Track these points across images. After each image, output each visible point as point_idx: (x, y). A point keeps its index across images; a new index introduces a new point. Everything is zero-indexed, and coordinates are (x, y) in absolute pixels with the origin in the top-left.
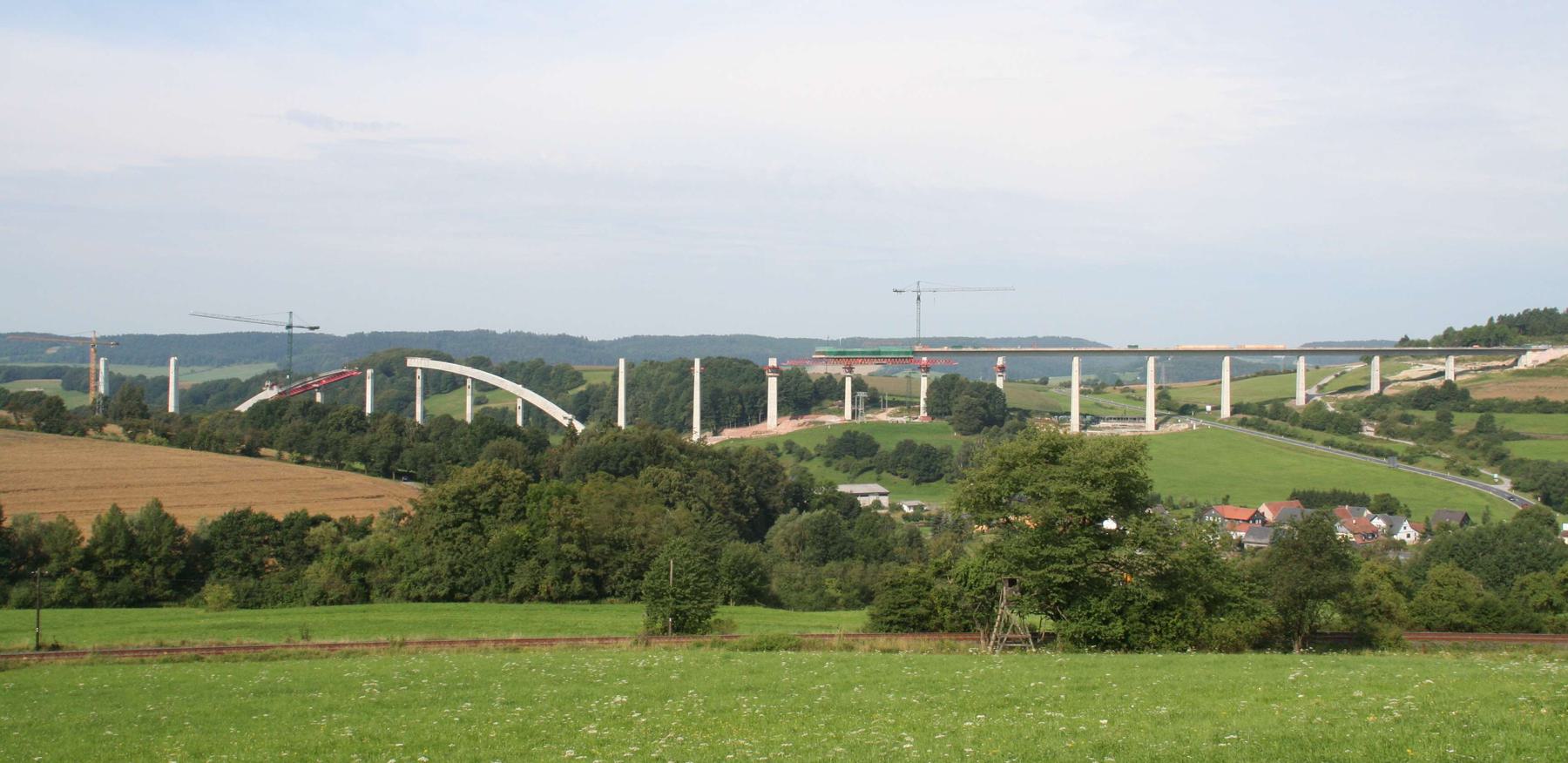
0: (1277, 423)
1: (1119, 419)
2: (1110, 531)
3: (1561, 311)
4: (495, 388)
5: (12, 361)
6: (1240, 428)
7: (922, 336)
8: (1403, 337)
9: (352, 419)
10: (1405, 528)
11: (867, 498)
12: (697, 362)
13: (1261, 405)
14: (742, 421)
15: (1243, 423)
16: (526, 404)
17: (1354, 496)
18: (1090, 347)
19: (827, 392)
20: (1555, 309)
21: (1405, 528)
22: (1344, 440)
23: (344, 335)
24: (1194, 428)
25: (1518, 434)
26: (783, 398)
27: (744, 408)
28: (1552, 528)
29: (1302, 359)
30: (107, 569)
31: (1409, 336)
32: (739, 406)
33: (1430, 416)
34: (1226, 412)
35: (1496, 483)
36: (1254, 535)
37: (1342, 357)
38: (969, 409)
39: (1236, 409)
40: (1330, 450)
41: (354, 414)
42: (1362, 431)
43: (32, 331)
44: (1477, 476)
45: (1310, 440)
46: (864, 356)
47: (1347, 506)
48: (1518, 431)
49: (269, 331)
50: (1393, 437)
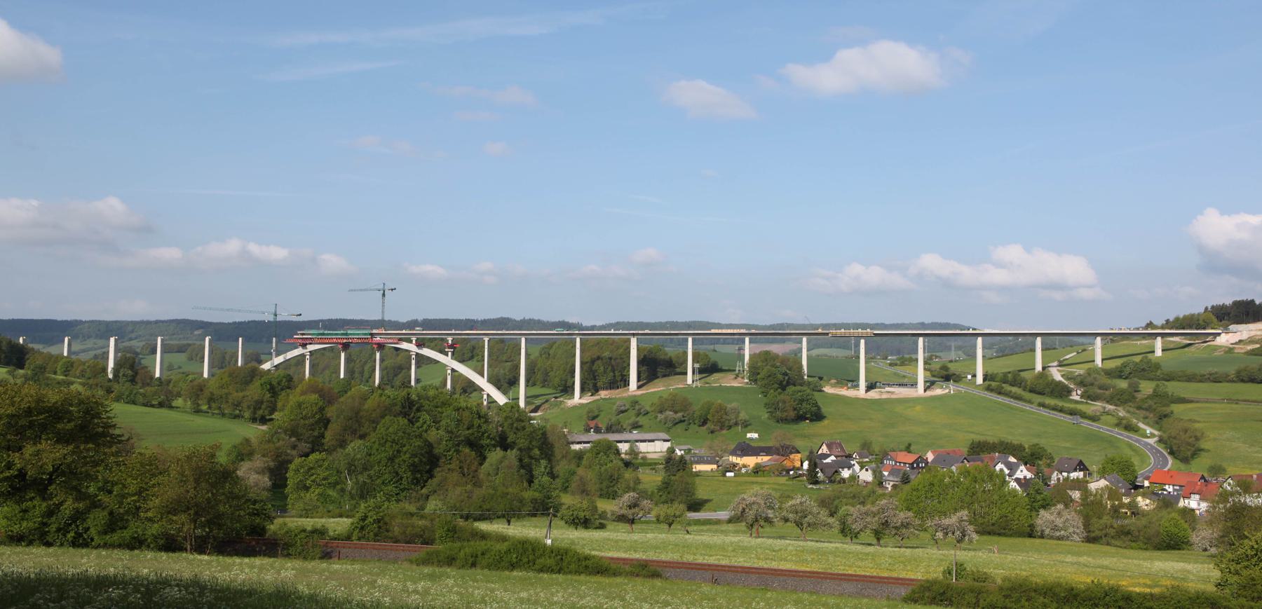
0: (1014, 389)
1: (900, 385)
2: (809, 465)
3: (1257, 302)
4: (437, 362)
5: (171, 339)
6: (986, 392)
7: (386, 318)
8: (1149, 322)
9: (282, 381)
10: (1022, 471)
11: (652, 443)
12: (634, 343)
13: (1005, 374)
14: (612, 385)
15: (989, 389)
16: (453, 370)
17: (1014, 446)
18: (582, 330)
19: (672, 367)
20: (1253, 301)
21: (1022, 471)
22: (1060, 403)
23: (405, 321)
24: (952, 392)
25: (1184, 398)
26: (625, 365)
27: (614, 376)
28: (414, 559)
29: (1099, 339)
30: (533, 451)
31: (1153, 321)
32: (612, 374)
33: (1123, 384)
34: (980, 380)
35: (1149, 437)
36: (893, 475)
37: (1136, 338)
38: (769, 376)
39: (986, 377)
40: (1044, 412)
41: (284, 377)
42: (1071, 395)
43: (222, 321)
44: (1136, 431)
45: (1030, 402)
46: (338, 337)
47: (997, 454)
48: (1185, 396)
49: (352, 318)
50: (1092, 400)
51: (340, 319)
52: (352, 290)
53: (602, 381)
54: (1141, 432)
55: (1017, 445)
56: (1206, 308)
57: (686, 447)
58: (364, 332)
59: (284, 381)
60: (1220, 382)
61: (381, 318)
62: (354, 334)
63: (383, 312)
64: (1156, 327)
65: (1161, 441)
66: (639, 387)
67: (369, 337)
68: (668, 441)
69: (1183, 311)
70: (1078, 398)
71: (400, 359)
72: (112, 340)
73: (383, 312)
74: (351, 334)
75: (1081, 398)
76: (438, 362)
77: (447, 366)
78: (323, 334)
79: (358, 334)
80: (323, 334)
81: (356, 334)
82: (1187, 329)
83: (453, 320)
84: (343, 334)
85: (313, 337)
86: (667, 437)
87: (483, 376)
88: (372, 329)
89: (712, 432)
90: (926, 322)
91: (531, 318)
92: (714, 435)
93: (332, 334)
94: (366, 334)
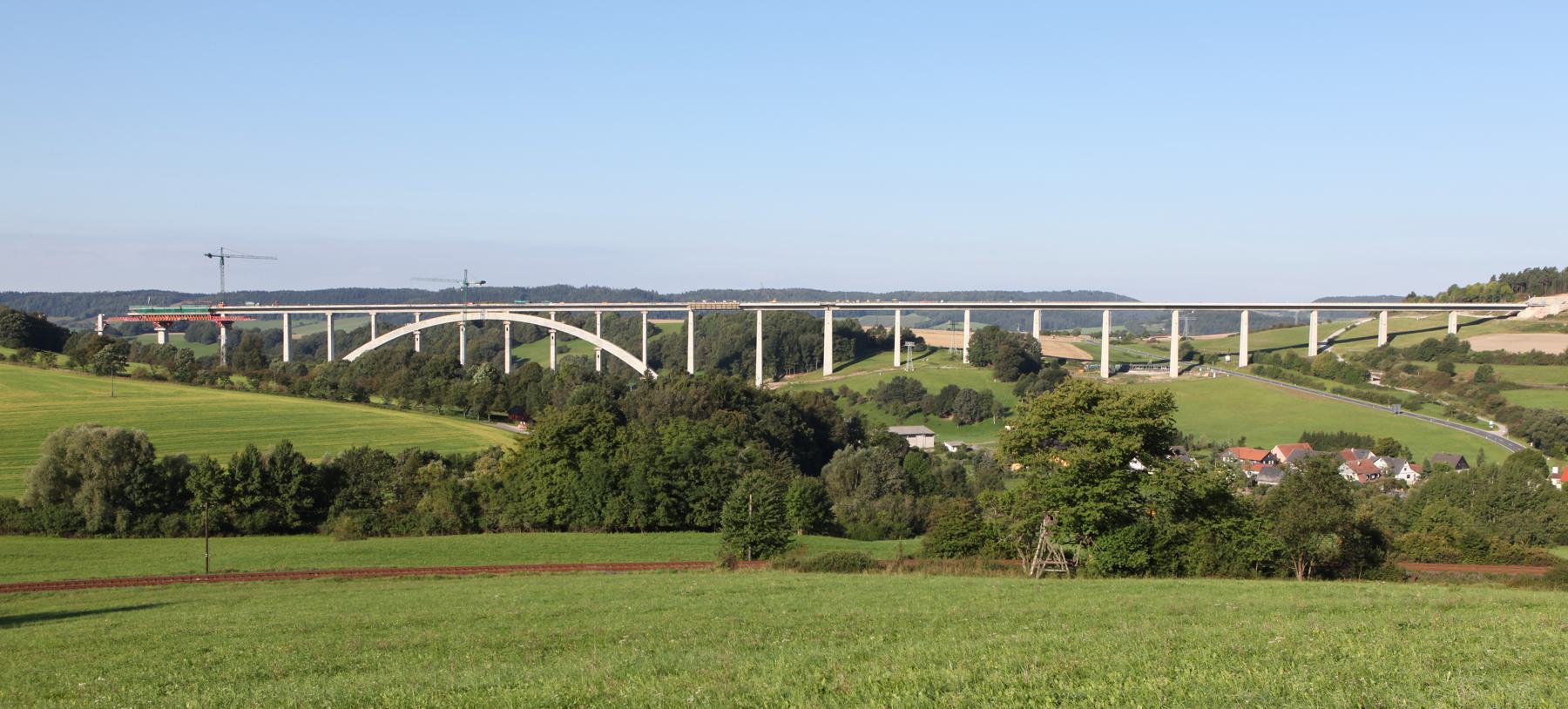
4: (576, 338)
6: (1257, 376)
10: (1405, 469)
20: (1555, 268)
21: (1405, 469)
33: (1432, 366)
34: (1243, 360)
35: (1492, 429)
44: (1474, 422)
51: (355, 289)
52: (272, 258)
53: (790, 362)
54: (1479, 423)
55: (1364, 437)
56: (1493, 278)
57: (959, 443)
58: (202, 308)
59: (452, 368)
60: (1547, 364)
61: (219, 291)
62: (190, 311)
63: (222, 283)
64: (1417, 299)
65: (1511, 432)
66: (835, 371)
67: (208, 313)
68: (931, 435)
69: (1466, 279)
70: (1377, 383)
71: (489, 339)
72: (100, 317)
73: (222, 283)
74: (186, 311)
75: (1381, 383)
76: (577, 338)
77: (596, 346)
78: (153, 311)
79: (195, 311)
80: (153, 311)
81: (191, 311)
82: (999, 301)
83: (498, 288)
84: (177, 311)
85: (141, 314)
86: (930, 432)
87: (641, 359)
88: (211, 305)
89: (962, 424)
90: (1073, 290)
91: (595, 285)
92: (964, 427)
93: (164, 311)
94: (203, 310)
